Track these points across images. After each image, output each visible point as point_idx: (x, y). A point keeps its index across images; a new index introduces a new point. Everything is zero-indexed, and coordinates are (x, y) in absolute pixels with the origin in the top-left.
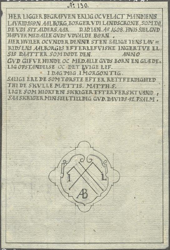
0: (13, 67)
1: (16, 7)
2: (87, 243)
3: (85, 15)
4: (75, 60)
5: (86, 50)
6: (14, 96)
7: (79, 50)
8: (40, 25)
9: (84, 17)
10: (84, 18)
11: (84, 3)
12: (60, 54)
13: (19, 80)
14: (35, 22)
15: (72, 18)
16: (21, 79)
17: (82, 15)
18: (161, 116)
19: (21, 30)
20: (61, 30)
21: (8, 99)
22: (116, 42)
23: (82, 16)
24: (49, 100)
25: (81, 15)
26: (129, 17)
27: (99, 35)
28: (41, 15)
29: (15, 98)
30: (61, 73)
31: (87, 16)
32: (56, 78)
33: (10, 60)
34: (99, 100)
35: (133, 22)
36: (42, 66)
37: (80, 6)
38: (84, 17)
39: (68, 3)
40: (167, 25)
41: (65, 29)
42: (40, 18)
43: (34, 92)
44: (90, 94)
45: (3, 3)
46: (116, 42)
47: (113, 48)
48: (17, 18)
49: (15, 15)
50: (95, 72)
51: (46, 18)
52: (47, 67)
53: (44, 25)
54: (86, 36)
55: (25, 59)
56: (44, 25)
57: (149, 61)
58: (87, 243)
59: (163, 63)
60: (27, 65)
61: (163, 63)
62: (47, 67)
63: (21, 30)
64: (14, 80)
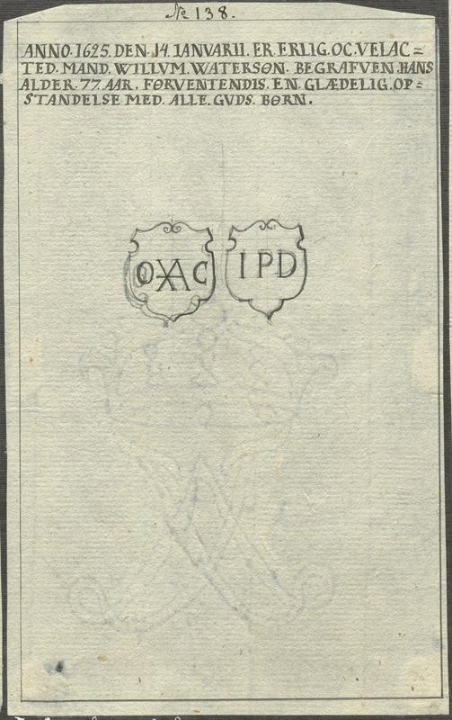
0: (376, 87)
1: (254, 703)
3: (302, 45)
4: (133, 97)
5: (173, 89)
8: (392, 72)
10: (298, 54)
12: (133, 100)
14: (162, 83)
15: (137, 55)
17: (291, 44)
21: (25, 103)
22: (303, 51)
23: (292, 49)
24: (138, 103)
25: (262, 46)
26: (130, 102)
28: (269, 45)
31: (308, 49)
33: (309, 82)
34: (229, 104)
35: (94, 66)
37: (204, 15)
38: (301, 53)
41: (122, 82)
42: (332, 70)
43: (70, 68)
48: (242, 71)
50: (268, 96)
54: (44, 85)
56: (25, 88)
57: (333, 85)
60: (104, 103)
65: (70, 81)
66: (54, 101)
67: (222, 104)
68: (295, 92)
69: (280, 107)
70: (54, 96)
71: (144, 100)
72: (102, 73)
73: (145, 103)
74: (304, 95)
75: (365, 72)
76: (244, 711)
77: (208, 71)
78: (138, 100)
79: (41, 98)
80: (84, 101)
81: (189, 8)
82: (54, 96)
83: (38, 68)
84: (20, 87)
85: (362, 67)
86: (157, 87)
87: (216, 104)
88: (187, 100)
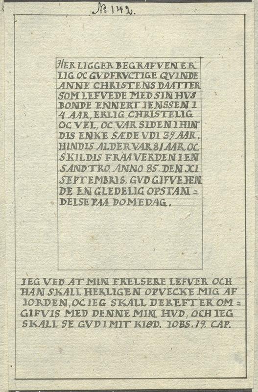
2: (246, 346)
4: (100, 177)
6: (101, 200)
7: (89, 183)
9: (107, 116)
11: (115, 4)
12: (113, 324)
13: (89, 67)
16: (149, 76)
18: (13, 123)
19: (61, 193)
20: (125, 158)
21: (60, 160)
22: (72, 293)
26: (68, 315)
27: (150, 323)
29: (170, 85)
30: (71, 75)
32: (226, 301)
36: (65, 189)
39: (94, 5)
40: (214, 386)
44: (108, 68)
45: (232, 372)
46: (72, 293)
47: (162, 281)
49: (71, 200)
51: (106, 182)
52: (75, 202)
53: (180, 137)
55: (83, 321)
56: (70, 170)
58: (246, 346)
59: (58, 187)
61: (58, 187)
62: (75, 202)
63: (61, 193)
64: (70, 293)
65: (141, 63)
66: (33, 293)
67: (135, 183)
68: (107, 287)
69: (133, 195)
70: (178, 188)
71: (29, 282)
72: (80, 149)
73: (140, 205)
74: (66, 300)
75: (172, 183)
76: (19, 4)
77: (122, 127)
78: (73, 314)
79: (137, 75)
80: (101, 314)
81: (132, 6)
82: (178, 188)
83: (137, 86)
84: (58, 87)
85: (171, 180)
86: (149, 326)
87: (120, 117)
88: (51, 324)
